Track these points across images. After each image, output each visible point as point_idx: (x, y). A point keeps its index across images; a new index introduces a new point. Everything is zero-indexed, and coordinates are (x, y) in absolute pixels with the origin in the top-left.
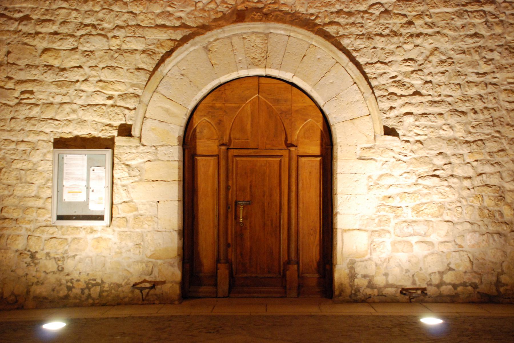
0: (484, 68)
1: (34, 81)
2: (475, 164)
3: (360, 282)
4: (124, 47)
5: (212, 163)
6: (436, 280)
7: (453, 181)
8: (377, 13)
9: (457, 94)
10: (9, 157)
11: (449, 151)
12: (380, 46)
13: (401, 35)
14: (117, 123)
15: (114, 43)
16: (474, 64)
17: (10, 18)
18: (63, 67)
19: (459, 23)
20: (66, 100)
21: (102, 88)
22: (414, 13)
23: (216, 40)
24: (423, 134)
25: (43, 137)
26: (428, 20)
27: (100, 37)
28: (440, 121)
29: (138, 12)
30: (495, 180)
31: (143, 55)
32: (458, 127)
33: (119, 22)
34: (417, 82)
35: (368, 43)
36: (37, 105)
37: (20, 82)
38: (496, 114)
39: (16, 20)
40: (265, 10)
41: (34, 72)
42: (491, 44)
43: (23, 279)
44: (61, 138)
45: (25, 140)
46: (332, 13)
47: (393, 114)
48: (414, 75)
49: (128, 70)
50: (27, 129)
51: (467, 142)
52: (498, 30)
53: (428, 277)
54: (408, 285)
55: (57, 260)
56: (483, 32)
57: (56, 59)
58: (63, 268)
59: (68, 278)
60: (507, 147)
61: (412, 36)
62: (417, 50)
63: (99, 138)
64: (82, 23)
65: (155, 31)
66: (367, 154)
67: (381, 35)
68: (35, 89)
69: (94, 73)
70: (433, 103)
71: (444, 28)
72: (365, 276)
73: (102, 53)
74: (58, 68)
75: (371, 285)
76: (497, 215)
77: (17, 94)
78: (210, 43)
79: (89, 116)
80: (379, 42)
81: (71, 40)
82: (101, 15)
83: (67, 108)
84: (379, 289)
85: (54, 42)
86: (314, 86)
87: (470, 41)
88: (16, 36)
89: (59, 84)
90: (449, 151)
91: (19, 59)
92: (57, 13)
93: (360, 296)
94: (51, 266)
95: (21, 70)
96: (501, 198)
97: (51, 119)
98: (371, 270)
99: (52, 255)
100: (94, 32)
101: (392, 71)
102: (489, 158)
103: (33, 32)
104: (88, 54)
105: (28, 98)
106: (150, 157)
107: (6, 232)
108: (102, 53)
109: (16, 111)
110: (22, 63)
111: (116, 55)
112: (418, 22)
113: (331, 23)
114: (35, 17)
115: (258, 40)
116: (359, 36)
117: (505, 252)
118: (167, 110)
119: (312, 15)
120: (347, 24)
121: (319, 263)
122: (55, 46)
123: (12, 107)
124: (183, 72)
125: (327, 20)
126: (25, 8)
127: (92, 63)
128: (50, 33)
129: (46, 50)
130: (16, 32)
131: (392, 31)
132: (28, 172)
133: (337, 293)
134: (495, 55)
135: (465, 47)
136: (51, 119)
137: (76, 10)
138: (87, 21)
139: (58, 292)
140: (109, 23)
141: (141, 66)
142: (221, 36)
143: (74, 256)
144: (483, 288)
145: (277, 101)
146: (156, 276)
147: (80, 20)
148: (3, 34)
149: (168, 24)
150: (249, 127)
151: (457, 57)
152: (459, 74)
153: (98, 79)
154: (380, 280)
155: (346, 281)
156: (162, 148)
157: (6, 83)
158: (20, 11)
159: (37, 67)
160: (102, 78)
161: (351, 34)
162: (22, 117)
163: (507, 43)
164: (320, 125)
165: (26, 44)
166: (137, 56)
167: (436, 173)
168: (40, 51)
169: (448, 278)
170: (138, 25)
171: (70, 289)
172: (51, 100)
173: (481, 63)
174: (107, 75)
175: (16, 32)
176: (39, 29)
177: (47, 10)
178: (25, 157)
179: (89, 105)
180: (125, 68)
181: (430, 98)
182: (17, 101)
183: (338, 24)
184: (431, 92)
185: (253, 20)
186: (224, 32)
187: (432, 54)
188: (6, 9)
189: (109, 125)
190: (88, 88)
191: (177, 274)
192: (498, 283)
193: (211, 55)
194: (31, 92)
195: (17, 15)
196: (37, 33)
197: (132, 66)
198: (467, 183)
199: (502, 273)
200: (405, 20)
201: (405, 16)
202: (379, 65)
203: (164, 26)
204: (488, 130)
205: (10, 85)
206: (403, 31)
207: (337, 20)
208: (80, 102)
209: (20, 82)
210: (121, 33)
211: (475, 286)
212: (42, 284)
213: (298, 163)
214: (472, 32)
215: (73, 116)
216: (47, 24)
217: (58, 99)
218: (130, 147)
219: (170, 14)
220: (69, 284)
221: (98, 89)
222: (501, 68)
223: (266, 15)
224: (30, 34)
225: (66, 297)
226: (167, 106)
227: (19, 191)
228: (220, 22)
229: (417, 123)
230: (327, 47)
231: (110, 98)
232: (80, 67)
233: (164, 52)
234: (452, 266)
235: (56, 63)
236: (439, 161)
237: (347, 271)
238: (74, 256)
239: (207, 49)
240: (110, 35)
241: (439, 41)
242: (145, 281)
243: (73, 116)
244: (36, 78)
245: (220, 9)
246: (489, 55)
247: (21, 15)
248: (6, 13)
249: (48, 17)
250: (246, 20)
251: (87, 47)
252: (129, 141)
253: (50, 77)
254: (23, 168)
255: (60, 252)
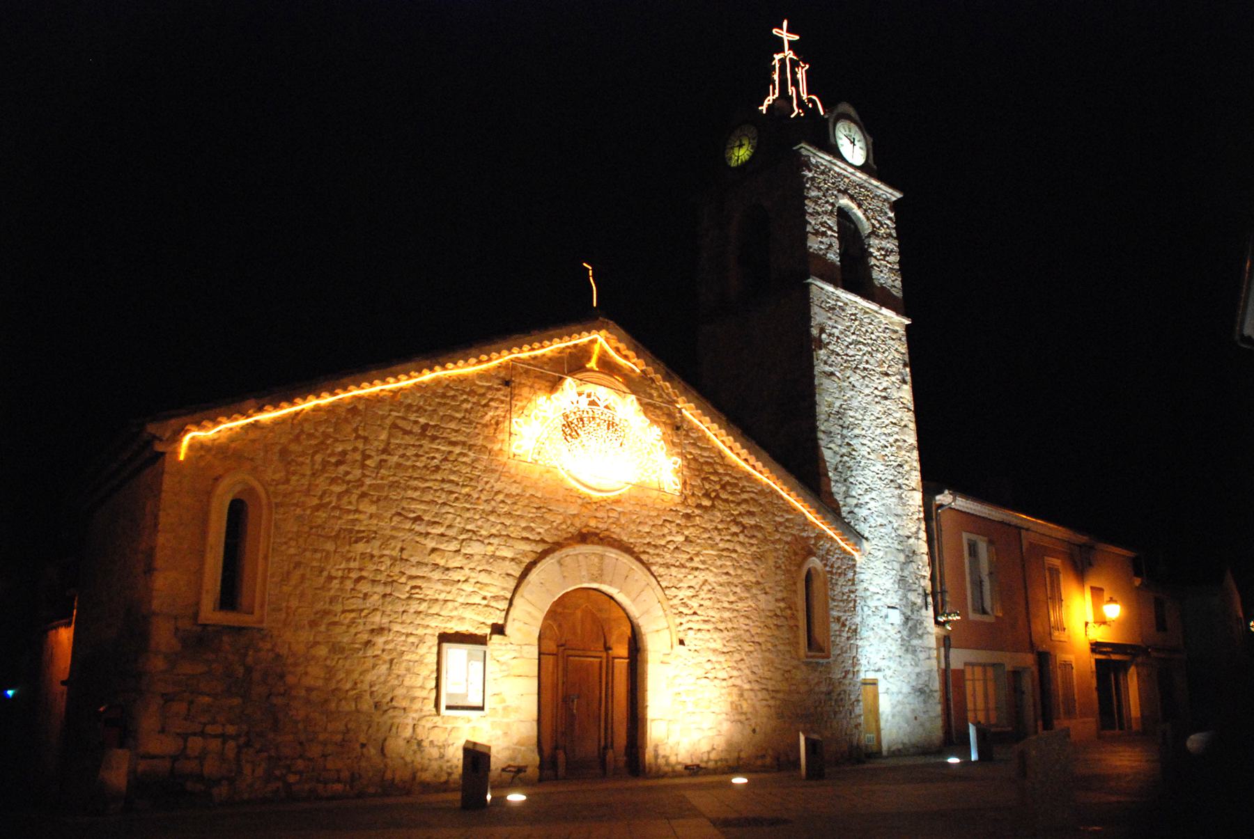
0: (732, 598)
1: (424, 577)
2: (728, 669)
3: (661, 761)
4: (498, 553)
5: (551, 661)
6: (705, 758)
7: (717, 682)
8: (672, 548)
9: (717, 616)
10: (399, 648)
11: (714, 659)
12: (674, 574)
13: (686, 567)
14: (490, 622)
15: (490, 549)
16: (726, 595)
17: (407, 518)
18: (447, 566)
19: (719, 563)
20: (449, 597)
21: (480, 589)
22: (694, 552)
23: (567, 556)
24: (701, 645)
25: (429, 631)
26: (702, 558)
27: (479, 543)
28: (708, 636)
29: (508, 524)
30: (738, 682)
31: (513, 563)
32: (719, 641)
33: (494, 531)
34: (694, 604)
35: (667, 571)
36: (425, 601)
37: (411, 578)
38: (739, 632)
39: (410, 519)
40: (601, 536)
41: (425, 570)
42: (736, 581)
43: (410, 766)
44: (444, 633)
45: (414, 632)
46: (644, 544)
47: (681, 628)
48: (693, 599)
49: (500, 575)
50: (416, 622)
51: (723, 653)
52: (739, 572)
53: (706, 755)
54: (689, 762)
55: (440, 747)
56: (732, 572)
57: (442, 559)
58: (444, 756)
59: (449, 764)
60: (745, 658)
61: (692, 569)
62: (696, 580)
63: (476, 635)
64: (464, 529)
65: (522, 542)
66: (666, 659)
67: (674, 565)
68: (424, 585)
69: (473, 575)
70: (705, 621)
71: (711, 565)
72: (664, 757)
73: (480, 557)
74: (443, 567)
75: (667, 764)
76: (739, 707)
77: (408, 588)
78: (562, 558)
79: (468, 614)
80: (673, 571)
81: (455, 542)
82: (479, 523)
83: (450, 605)
84: (673, 767)
85: (442, 543)
86: (634, 601)
87: (725, 577)
88: (410, 534)
89: (445, 582)
90: (714, 659)
91: (412, 556)
92: (445, 516)
93: (661, 773)
94: (435, 753)
95: (413, 566)
96: (741, 695)
97: (437, 614)
98: (667, 752)
99: (436, 743)
100: (474, 538)
101: (681, 594)
102: (735, 665)
103: (424, 532)
104: (469, 557)
105: (417, 593)
106: (515, 654)
107: (397, 721)
108: (480, 557)
109: (408, 605)
110: (414, 560)
111: (491, 560)
112: (696, 559)
113: (644, 552)
114: (426, 518)
115: (596, 560)
116: (662, 565)
117: (743, 734)
118: (529, 613)
119: (631, 543)
120: (654, 554)
121: (627, 747)
122: (442, 547)
123: (404, 600)
124: (542, 581)
125: (642, 550)
126: (418, 509)
127: (472, 565)
128: (438, 535)
129: (434, 550)
130: (411, 530)
131: (681, 563)
132: (416, 664)
133: (647, 770)
134: (738, 590)
135: (722, 581)
136: (437, 614)
137: (459, 515)
138: (469, 527)
139: (440, 777)
140: (486, 530)
141: (510, 572)
142: (571, 553)
143: (453, 744)
144: (730, 763)
145: (600, 610)
146: (519, 762)
147: (462, 525)
148: (400, 532)
149: (531, 537)
150: (579, 632)
151: (718, 588)
152: (719, 601)
153: (476, 580)
154: (673, 759)
155: (652, 761)
156: (526, 647)
157: (400, 578)
158: (414, 512)
159: (427, 564)
160: (480, 580)
161: (657, 562)
162: (412, 611)
163: (744, 582)
164: (629, 632)
165: (417, 542)
166: (507, 563)
167: (707, 675)
168: (429, 550)
169: (713, 756)
170: (508, 536)
171: (449, 774)
172: (437, 596)
173: (731, 594)
174: (483, 578)
175: (411, 530)
176: (430, 530)
177: (436, 513)
178: (413, 648)
179: (467, 604)
180: (498, 573)
181: (702, 618)
182: (407, 595)
183: (648, 553)
184: (703, 613)
185: (593, 543)
186: (575, 550)
187: (704, 584)
188: (403, 509)
189: (483, 623)
190: (468, 587)
191: (537, 758)
192: (739, 758)
193: (563, 569)
194: (420, 587)
195: (412, 515)
196: (428, 534)
197: (504, 572)
198: (724, 683)
199: (741, 751)
200: (688, 557)
201: (688, 553)
202: (673, 589)
203: (527, 539)
204: (734, 644)
205: (403, 580)
206: (688, 564)
207: (647, 550)
208: (461, 600)
209: (411, 578)
210: (495, 541)
211: (726, 760)
212: (426, 770)
213: (613, 663)
214: (725, 571)
215: (454, 613)
216: (436, 526)
217: (442, 596)
218: (500, 644)
219: (533, 530)
220: (449, 770)
221: (475, 589)
222: (741, 599)
223: (601, 539)
224: (421, 534)
225: (446, 782)
226: (530, 610)
227: (407, 682)
228: (569, 541)
229: (696, 636)
230: (643, 572)
231: (484, 598)
232: (461, 568)
233: (528, 561)
234: (715, 747)
235: (442, 562)
236: (709, 666)
237: (653, 753)
238: (453, 744)
239: (560, 563)
240: (486, 541)
241: (707, 575)
242: (509, 766)
243: (454, 613)
244: (425, 575)
245: (570, 530)
246: (735, 589)
247: (414, 515)
248: (403, 513)
249: (437, 520)
250: (588, 541)
251: (468, 551)
252: (503, 639)
253: (436, 575)
254: (412, 659)
255: (441, 740)
